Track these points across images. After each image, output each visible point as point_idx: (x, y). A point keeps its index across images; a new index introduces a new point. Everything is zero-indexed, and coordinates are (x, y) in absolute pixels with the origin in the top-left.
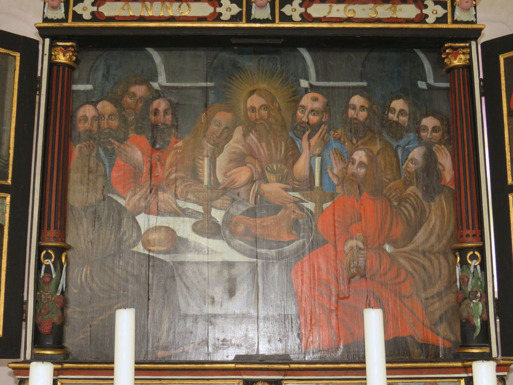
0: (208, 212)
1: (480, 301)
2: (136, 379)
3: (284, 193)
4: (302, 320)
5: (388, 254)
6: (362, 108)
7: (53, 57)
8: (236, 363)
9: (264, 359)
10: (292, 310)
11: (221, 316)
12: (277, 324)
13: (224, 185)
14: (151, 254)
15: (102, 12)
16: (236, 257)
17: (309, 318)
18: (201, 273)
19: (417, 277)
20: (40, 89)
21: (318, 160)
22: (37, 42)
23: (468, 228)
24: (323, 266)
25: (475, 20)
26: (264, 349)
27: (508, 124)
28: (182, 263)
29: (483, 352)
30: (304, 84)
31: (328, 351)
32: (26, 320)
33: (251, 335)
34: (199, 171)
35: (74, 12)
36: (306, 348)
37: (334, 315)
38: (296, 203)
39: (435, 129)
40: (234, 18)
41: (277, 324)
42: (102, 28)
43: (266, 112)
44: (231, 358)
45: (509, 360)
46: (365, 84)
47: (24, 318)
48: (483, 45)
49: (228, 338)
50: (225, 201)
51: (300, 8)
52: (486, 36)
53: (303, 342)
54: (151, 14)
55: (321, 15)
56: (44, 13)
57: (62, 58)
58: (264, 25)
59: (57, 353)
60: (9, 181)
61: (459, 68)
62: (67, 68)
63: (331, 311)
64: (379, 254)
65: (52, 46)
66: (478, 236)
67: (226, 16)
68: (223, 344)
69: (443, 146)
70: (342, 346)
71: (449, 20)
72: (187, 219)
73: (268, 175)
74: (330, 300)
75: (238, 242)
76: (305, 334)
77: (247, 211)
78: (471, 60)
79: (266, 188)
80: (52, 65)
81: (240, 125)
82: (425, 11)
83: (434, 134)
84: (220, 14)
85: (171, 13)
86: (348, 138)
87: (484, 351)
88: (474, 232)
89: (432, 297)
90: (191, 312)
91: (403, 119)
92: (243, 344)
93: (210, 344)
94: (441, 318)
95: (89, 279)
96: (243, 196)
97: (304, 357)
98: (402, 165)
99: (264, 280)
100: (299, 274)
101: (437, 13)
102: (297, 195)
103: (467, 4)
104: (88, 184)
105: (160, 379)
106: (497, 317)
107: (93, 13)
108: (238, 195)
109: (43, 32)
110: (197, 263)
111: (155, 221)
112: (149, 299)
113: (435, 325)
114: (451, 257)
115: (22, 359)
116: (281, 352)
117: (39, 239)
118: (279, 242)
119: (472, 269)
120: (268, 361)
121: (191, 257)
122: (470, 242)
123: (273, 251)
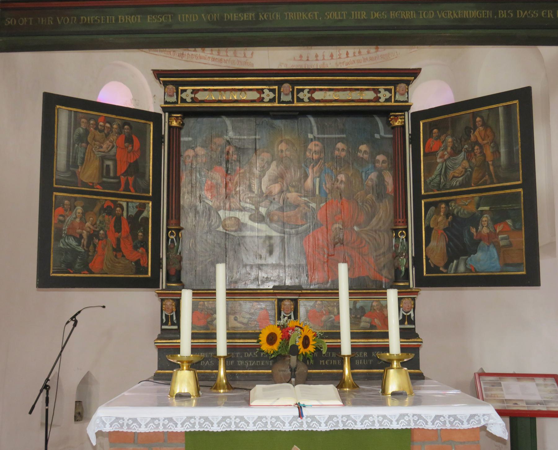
0: (257, 209)
1: (405, 257)
2: (227, 298)
3: (299, 198)
4: (309, 267)
5: (356, 231)
6: (343, 150)
7: (170, 123)
8: (274, 290)
9: (288, 288)
10: (303, 262)
11: (265, 265)
12: (295, 269)
13: (267, 194)
14: (227, 232)
15: (197, 98)
16: (274, 234)
17: (312, 266)
18: (254, 242)
19: (371, 244)
20: (164, 142)
21: (318, 180)
22: (161, 115)
23: (400, 218)
24: (320, 238)
25: (407, 100)
26: (288, 282)
27: (423, 161)
28: (244, 237)
29: (405, 285)
30: (310, 136)
31: (322, 283)
32: (162, 268)
33: (281, 275)
34: (252, 186)
35: (181, 98)
36: (311, 282)
37: (326, 265)
38: (305, 204)
39: (383, 162)
40: (272, 100)
41: (295, 269)
42: (197, 107)
43: (289, 153)
44: (271, 287)
45: (418, 289)
46: (344, 136)
47: (161, 267)
48: (413, 114)
49: (269, 277)
50: (266, 203)
51: (308, 94)
52: (412, 110)
53: (309, 279)
54: (224, 98)
55: (320, 98)
56: (165, 99)
57: (174, 124)
58: (288, 105)
59: (178, 285)
60: (151, 194)
61: (398, 127)
62: (178, 129)
63: (324, 263)
64: (351, 232)
65: (170, 117)
66: (405, 222)
67: (266, 99)
68: (266, 280)
69: (388, 171)
70: (330, 281)
71: (393, 100)
72: (246, 213)
73: (290, 188)
74: (324, 256)
75: (274, 225)
76: (310, 275)
77: (279, 208)
78: (404, 122)
79: (289, 195)
80: (170, 127)
81: (275, 160)
82: (379, 95)
83: (383, 165)
84: (263, 98)
85: (235, 98)
86: (335, 167)
87: (406, 284)
88: (403, 220)
89: (380, 255)
90: (248, 263)
91: (366, 156)
92: (277, 280)
93: (259, 280)
94: (384, 266)
95: (194, 246)
96: (276, 200)
97: (310, 287)
98: (365, 182)
99: (288, 246)
100: (307, 242)
101: (386, 96)
102: (306, 199)
103: (403, 92)
104: (191, 194)
105: (234, 298)
106: (414, 266)
107: (192, 98)
108: (274, 199)
109: (164, 109)
110: (252, 237)
111: (228, 214)
112: (226, 256)
113: (381, 270)
114: (390, 233)
115: (161, 288)
116: (297, 284)
117: (167, 225)
118: (297, 225)
119: (401, 240)
120: (290, 289)
121: (248, 233)
122: (400, 226)
123: (293, 230)
